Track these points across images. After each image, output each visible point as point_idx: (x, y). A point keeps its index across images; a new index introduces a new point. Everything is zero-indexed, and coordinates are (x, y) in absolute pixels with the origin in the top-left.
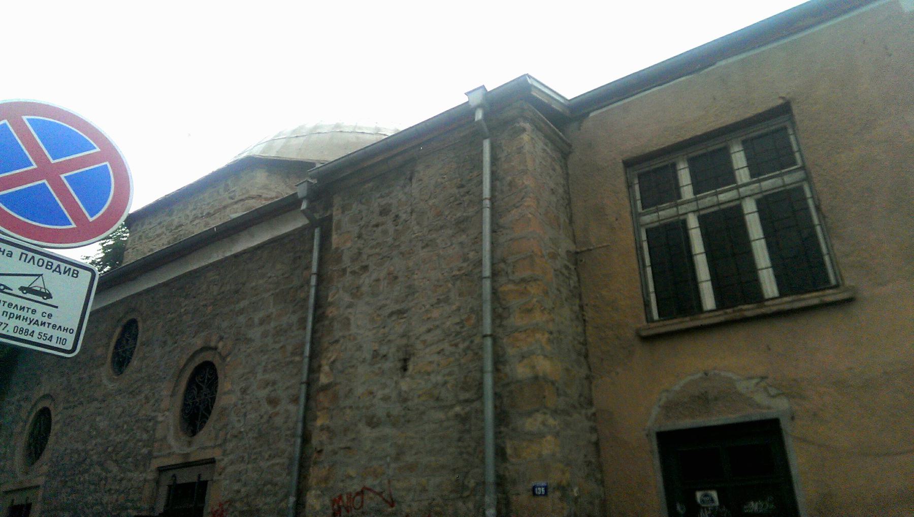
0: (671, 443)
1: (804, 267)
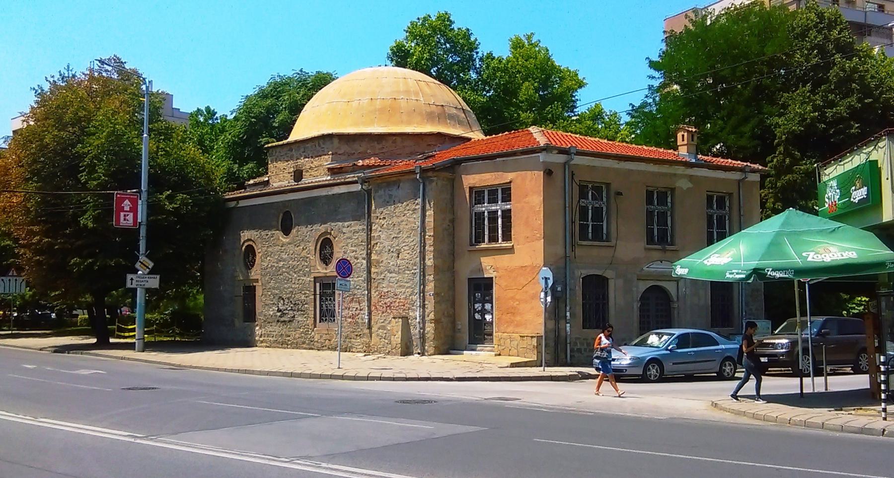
0: (470, 280)
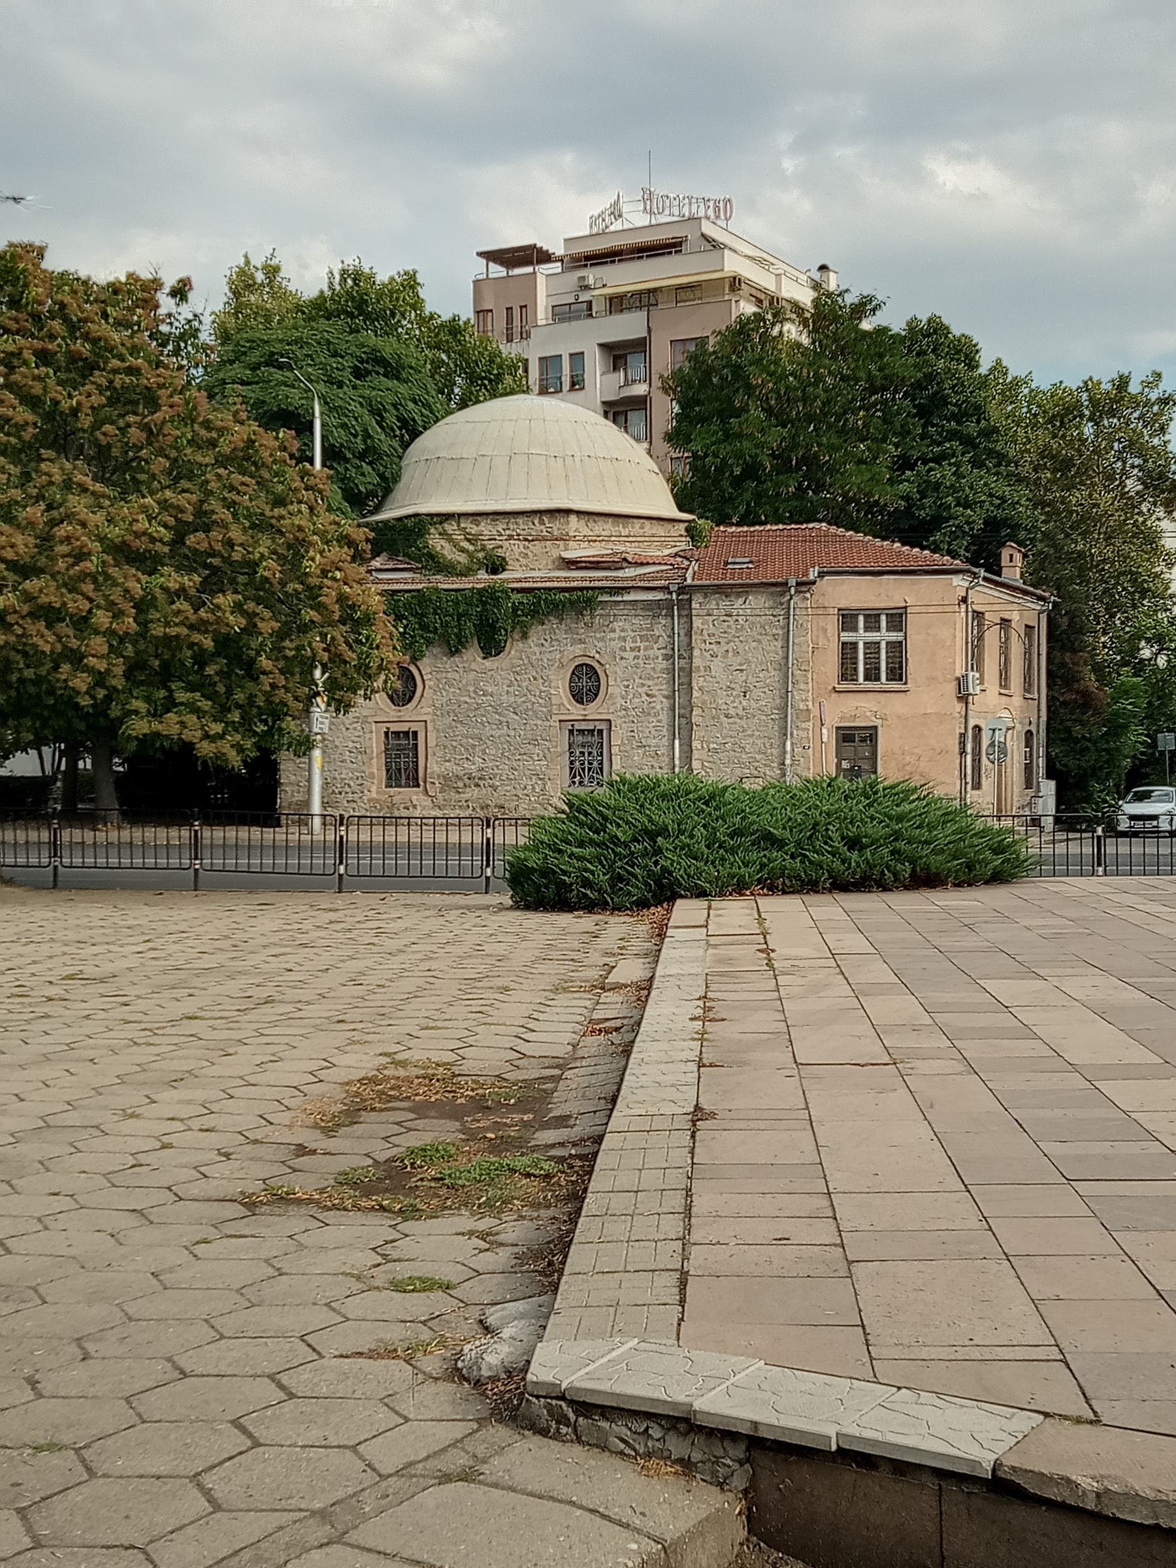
1: (897, 673)
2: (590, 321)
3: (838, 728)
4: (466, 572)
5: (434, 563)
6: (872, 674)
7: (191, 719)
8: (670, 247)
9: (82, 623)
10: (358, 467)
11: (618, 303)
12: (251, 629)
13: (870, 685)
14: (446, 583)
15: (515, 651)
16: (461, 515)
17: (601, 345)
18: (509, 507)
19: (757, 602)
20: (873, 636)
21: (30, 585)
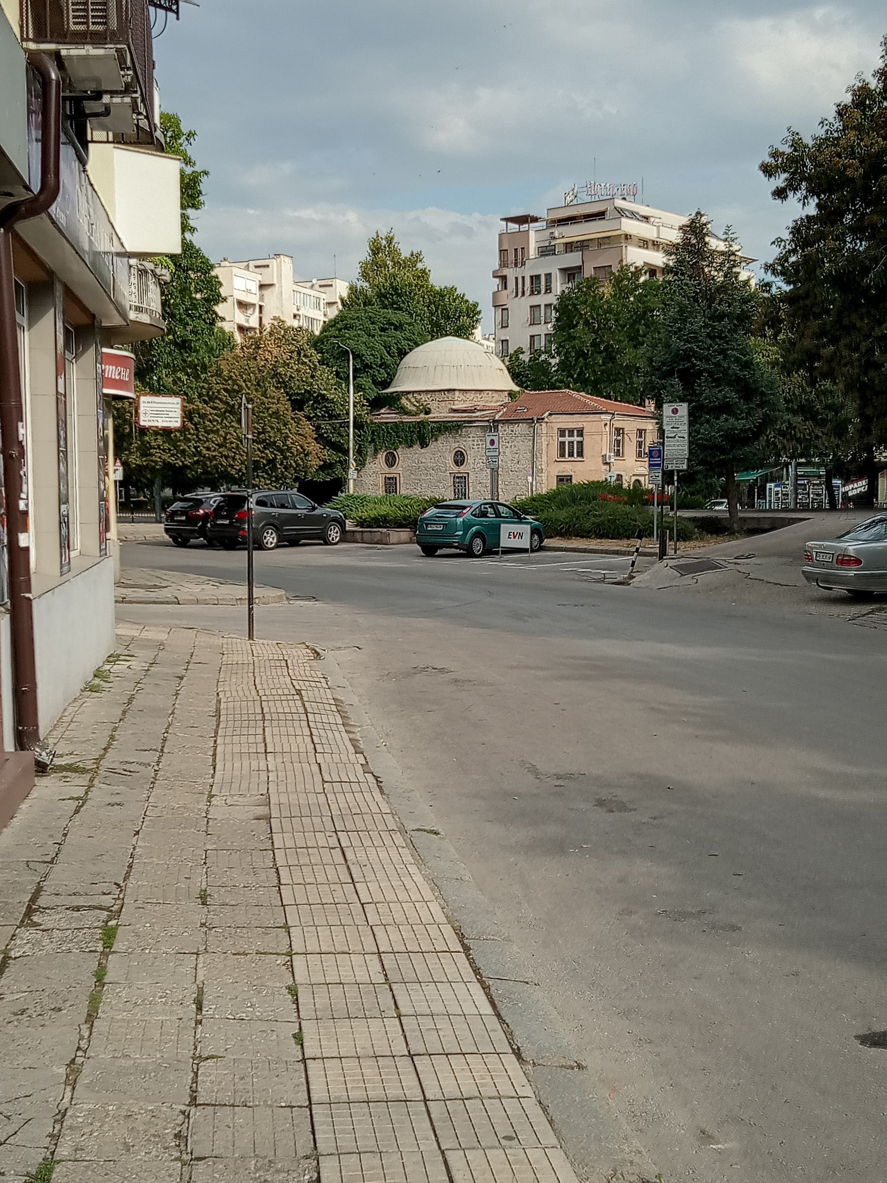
1: (580, 454)
2: (554, 257)
3: (558, 476)
4: (416, 414)
5: (404, 411)
6: (571, 454)
7: (262, 480)
8: (601, 215)
9: (234, 459)
10: (379, 371)
11: (570, 247)
12: (275, 458)
13: (570, 459)
14: (406, 419)
15: (433, 445)
16: (413, 392)
17: (560, 269)
18: (432, 389)
19: (522, 428)
20: (571, 439)
21: (221, 450)
